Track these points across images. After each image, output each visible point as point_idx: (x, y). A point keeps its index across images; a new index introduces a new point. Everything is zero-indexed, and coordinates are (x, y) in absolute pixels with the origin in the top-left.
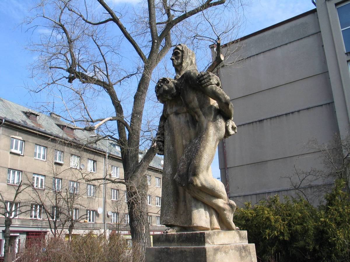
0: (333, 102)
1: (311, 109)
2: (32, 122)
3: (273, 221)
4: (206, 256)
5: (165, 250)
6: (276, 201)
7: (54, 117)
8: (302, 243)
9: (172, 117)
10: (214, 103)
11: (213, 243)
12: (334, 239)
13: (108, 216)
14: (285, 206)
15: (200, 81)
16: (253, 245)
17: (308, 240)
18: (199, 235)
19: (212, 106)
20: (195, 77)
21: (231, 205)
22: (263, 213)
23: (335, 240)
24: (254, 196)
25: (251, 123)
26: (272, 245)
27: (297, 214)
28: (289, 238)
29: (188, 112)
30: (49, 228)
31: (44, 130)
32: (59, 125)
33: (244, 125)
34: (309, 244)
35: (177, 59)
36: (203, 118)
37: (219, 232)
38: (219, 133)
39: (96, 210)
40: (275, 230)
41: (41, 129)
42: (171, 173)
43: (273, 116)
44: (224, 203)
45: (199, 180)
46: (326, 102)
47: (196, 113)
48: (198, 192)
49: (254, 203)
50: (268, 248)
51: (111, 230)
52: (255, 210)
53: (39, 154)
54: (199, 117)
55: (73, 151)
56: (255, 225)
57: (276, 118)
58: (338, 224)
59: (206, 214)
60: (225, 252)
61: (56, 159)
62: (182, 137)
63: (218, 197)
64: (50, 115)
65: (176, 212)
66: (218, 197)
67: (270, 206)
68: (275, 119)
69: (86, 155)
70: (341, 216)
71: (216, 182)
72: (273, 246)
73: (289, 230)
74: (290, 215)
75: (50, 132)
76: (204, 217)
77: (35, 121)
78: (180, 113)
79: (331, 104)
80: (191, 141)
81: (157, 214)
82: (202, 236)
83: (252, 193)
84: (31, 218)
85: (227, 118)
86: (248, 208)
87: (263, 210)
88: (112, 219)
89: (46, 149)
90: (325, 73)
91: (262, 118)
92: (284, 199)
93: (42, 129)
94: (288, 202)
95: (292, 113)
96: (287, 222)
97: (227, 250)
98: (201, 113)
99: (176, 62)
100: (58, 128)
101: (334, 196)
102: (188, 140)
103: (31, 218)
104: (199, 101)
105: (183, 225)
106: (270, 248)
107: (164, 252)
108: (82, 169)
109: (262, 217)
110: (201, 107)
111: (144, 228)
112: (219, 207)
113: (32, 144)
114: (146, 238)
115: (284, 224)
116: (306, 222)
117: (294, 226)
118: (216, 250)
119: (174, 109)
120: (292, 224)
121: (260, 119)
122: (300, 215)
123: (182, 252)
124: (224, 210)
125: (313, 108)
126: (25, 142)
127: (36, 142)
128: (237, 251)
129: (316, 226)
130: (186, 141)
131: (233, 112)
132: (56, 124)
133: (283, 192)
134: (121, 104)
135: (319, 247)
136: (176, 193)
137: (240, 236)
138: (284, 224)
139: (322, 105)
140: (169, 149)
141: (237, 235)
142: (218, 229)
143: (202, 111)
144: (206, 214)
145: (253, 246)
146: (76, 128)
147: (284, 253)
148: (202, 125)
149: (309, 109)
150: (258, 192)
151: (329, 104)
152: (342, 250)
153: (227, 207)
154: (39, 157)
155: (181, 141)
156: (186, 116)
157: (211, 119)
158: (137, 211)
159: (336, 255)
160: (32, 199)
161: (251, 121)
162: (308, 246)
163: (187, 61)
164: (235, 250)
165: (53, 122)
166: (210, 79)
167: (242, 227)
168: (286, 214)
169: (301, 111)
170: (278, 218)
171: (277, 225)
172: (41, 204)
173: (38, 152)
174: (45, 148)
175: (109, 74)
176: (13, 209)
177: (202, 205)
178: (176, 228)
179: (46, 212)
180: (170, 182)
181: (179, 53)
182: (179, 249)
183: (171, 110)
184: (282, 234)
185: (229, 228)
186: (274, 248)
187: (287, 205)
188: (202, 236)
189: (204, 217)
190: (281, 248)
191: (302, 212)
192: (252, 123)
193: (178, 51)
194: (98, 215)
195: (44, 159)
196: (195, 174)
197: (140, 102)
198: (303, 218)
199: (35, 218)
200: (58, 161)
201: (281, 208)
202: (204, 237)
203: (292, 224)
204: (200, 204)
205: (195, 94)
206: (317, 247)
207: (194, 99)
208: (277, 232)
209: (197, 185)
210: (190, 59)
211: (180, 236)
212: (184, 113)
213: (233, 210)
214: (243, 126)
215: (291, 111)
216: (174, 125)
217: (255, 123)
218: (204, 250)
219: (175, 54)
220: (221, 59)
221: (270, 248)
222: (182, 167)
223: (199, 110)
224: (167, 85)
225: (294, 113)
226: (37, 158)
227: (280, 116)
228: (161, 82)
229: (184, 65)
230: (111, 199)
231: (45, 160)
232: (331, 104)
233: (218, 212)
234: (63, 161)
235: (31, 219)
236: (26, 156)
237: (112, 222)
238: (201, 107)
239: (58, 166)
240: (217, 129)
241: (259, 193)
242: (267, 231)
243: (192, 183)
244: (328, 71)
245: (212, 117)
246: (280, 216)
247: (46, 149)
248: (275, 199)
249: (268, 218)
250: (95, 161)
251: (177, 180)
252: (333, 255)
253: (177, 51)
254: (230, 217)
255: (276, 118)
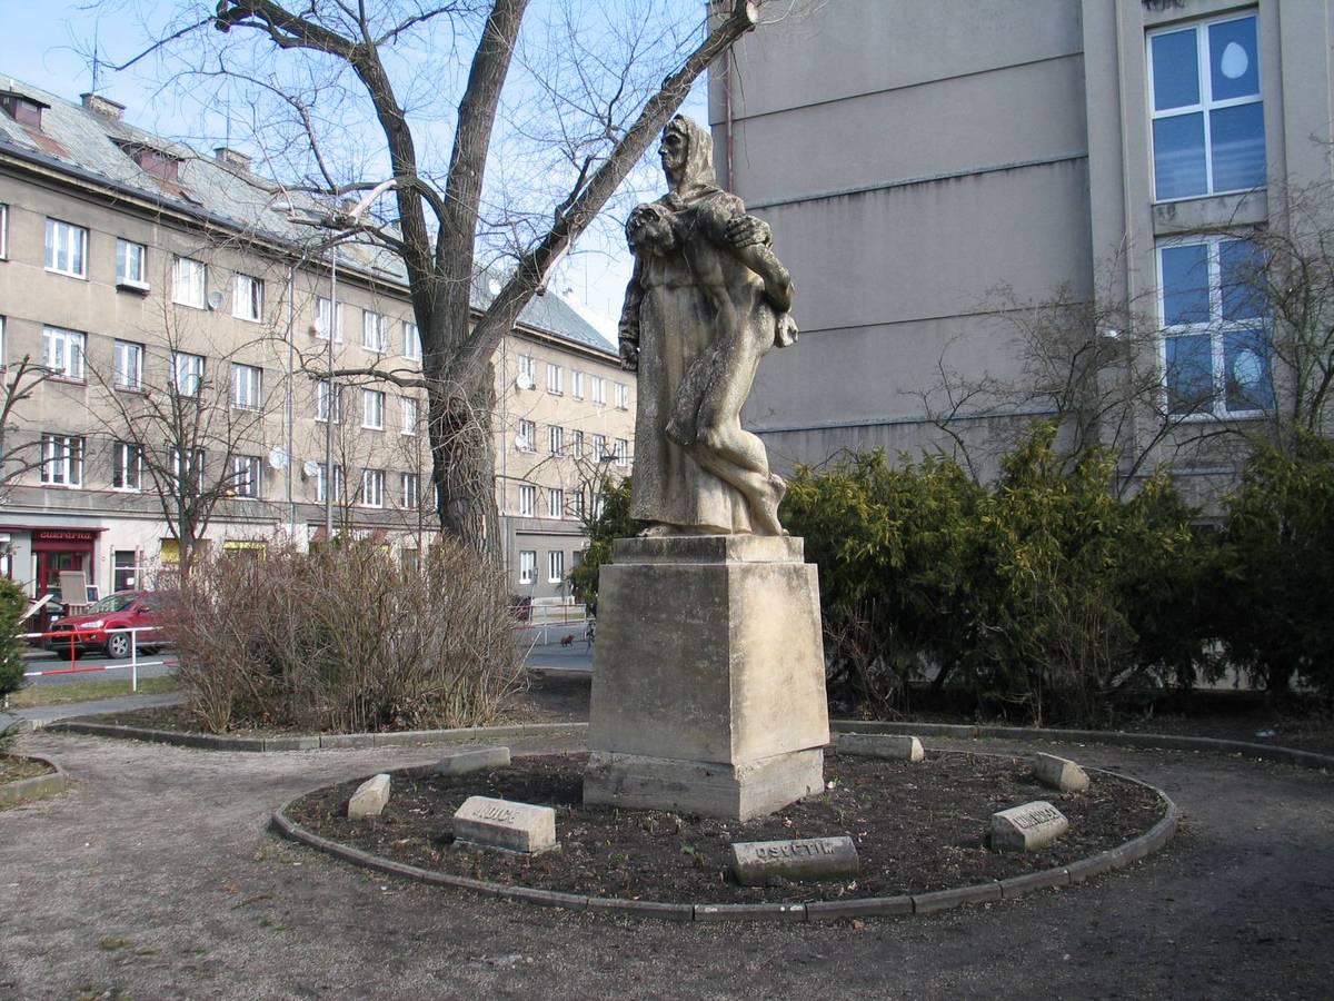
0: (1085, 157)
1: (1018, 171)
2: (27, 132)
3: (864, 516)
4: (727, 580)
5: (644, 570)
6: (878, 465)
7: (98, 110)
8: (931, 575)
9: (661, 294)
10: (755, 279)
11: (739, 558)
12: (1006, 568)
13: (304, 478)
14: (899, 480)
15: (732, 236)
16: (814, 567)
17: (947, 569)
18: (714, 543)
19: (750, 286)
20: (722, 227)
21: (775, 486)
22: (843, 495)
23: (1010, 570)
24: (818, 435)
25: (822, 198)
26: (859, 578)
27: (927, 502)
28: (901, 560)
29: (697, 285)
30: (163, 520)
31: (73, 163)
32: (117, 142)
33: (799, 202)
34: (947, 578)
35: (674, 153)
36: (730, 307)
37: (750, 539)
38: (763, 342)
39: (263, 456)
40: (869, 541)
41: (63, 160)
42: (656, 415)
43: (896, 181)
44: (763, 482)
45: (719, 435)
46: (1064, 154)
47: (718, 295)
48: (714, 459)
49: (812, 452)
50: (846, 584)
51: (315, 525)
52: (820, 484)
53: (63, 256)
54: (722, 303)
55: (182, 242)
56: (818, 525)
57: (905, 189)
58: (1024, 534)
59: (725, 501)
60: (761, 576)
61: (121, 271)
62: (682, 341)
63: (752, 468)
64: (81, 99)
65: (665, 496)
66: (752, 468)
67: (859, 478)
68: (900, 193)
69: (223, 258)
70: (1034, 513)
71: (751, 443)
72: (860, 582)
73: (904, 542)
74: (910, 504)
75: (95, 171)
76: (721, 508)
77: (35, 128)
78: (678, 287)
79: (1080, 161)
80: (700, 352)
81: (523, 480)
82: (720, 544)
83: (810, 425)
84: (43, 483)
85: (779, 309)
86: (800, 479)
87: (844, 487)
88: (316, 490)
89: (85, 235)
90: (1075, 56)
91: (861, 186)
92: (900, 459)
93: (69, 162)
94: (908, 468)
95: (958, 178)
96: (901, 522)
97: (764, 573)
98: (726, 296)
99: (671, 161)
100: (121, 154)
101: (1025, 462)
102: (695, 349)
103: (43, 483)
104: (725, 271)
105: (676, 523)
106: (852, 586)
107: (639, 574)
108: (215, 308)
109: (839, 505)
110: (729, 285)
111: (484, 523)
112: (753, 489)
113: (35, 218)
114: (490, 554)
115: (892, 526)
116: (948, 524)
117: (917, 533)
118: (746, 571)
119: (667, 276)
120: (913, 527)
121: (853, 188)
122: (933, 504)
123: (679, 574)
124: (762, 494)
125: (1025, 169)
126: (11, 210)
127: (49, 210)
128: (784, 576)
129: (970, 535)
130: (690, 348)
131: (792, 300)
132: (110, 137)
133: (906, 427)
134: (407, 119)
135: (972, 585)
136: (665, 457)
137: (789, 547)
138: (893, 526)
139: (1051, 163)
140: (652, 362)
141: (785, 546)
142: (747, 532)
143: (729, 294)
144: (725, 501)
145: (812, 570)
146: (297, 218)
147: (887, 600)
148: (729, 322)
149: (1011, 172)
150: (829, 422)
151: (1074, 160)
152: (1024, 595)
153: (768, 489)
154: (62, 266)
155: (678, 349)
156: (692, 295)
157: (748, 314)
158: (462, 472)
159: (1009, 607)
160: (101, 424)
161: (823, 192)
162: (946, 583)
163: (696, 161)
164: (779, 573)
165: (97, 132)
166: (753, 233)
167: (794, 529)
168: (901, 501)
169: (984, 175)
170: (879, 511)
171: (875, 527)
172: (132, 439)
173: (56, 246)
174: (82, 234)
175: (368, 14)
176: (51, 454)
177: (719, 485)
178: (663, 529)
179: (152, 468)
180: (653, 433)
181: (679, 141)
182: (674, 569)
183: (659, 277)
184: (886, 551)
185: (770, 532)
186: (863, 587)
187: (906, 477)
188: (720, 544)
189: (721, 508)
190: (881, 587)
191: (942, 499)
192: (828, 197)
193: (677, 135)
194: (270, 473)
195: (80, 272)
196: (711, 423)
197: (480, 126)
198: (943, 513)
199: (57, 484)
200: (129, 281)
201: (888, 483)
202: (724, 547)
203: (913, 527)
204: (713, 481)
205: (718, 258)
206: (967, 588)
207: (714, 267)
208: (874, 546)
209: (713, 445)
210: (702, 154)
211: (675, 544)
212: (687, 286)
213: (779, 496)
214: (796, 207)
215: (954, 172)
216: (666, 313)
217: (836, 200)
218: (726, 570)
219: (669, 141)
220: (747, 18)
221: (852, 586)
222: (684, 406)
223: (723, 291)
224: (654, 226)
225: (964, 179)
226: (55, 269)
227: (918, 183)
228: (640, 216)
229: (688, 170)
230: (316, 418)
231: (83, 277)
232: (1078, 161)
233: (749, 498)
234: (145, 281)
235: (43, 487)
236: (17, 263)
237: (316, 497)
238: (729, 285)
239: (129, 299)
240: (759, 334)
241: (833, 425)
242: (850, 543)
243: (704, 441)
244: (1083, 53)
245: (751, 308)
246: (885, 504)
247: (85, 235)
248: (875, 459)
249: (853, 510)
250: (258, 282)
251: (673, 432)
252: (1002, 606)
253: (674, 136)
254: (772, 508)
255: (905, 189)
